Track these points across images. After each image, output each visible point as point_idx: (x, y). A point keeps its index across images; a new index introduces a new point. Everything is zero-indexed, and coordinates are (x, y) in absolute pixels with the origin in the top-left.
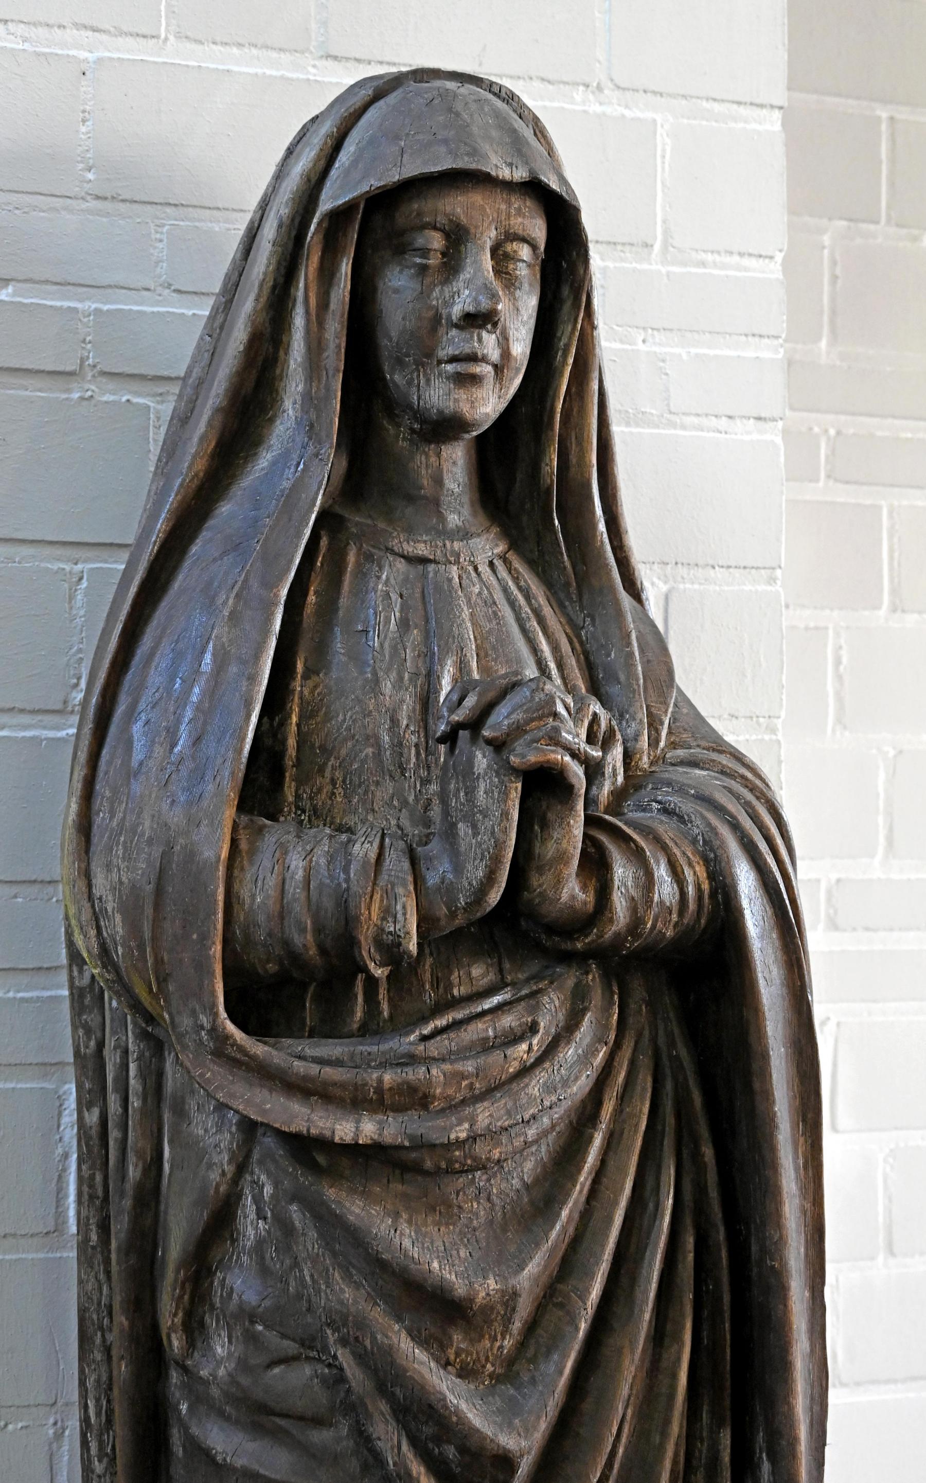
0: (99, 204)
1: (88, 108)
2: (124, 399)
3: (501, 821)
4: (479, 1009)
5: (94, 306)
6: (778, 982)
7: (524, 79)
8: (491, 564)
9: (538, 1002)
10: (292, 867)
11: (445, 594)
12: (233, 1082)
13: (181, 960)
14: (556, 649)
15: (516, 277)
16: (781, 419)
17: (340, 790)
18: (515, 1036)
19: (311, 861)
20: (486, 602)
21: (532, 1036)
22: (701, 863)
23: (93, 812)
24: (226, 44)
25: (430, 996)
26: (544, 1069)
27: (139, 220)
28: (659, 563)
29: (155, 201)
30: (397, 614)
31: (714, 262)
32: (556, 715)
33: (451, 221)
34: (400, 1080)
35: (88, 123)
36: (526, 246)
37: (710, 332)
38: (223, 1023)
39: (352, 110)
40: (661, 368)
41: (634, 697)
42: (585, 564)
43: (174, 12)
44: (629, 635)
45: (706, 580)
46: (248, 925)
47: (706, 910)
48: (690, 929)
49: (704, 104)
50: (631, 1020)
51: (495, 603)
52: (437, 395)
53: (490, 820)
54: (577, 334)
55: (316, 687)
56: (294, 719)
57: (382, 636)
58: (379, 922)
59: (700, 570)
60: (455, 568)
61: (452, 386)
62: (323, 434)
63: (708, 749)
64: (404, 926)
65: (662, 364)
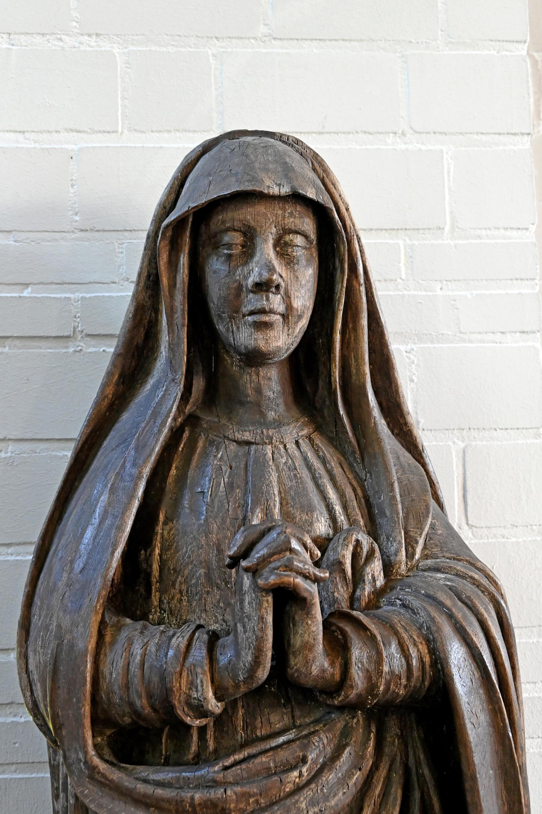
0: (83, 234)
1: (74, 178)
2: (101, 350)
3: (259, 623)
4: (268, 747)
5: (81, 295)
6: (485, 724)
7: (352, 133)
8: (297, 443)
9: (309, 742)
10: (134, 653)
11: (261, 464)
12: (102, 797)
13: (68, 715)
14: (342, 496)
15: (294, 257)
16: (538, 331)
17: (185, 598)
18: (291, 766)
19: (146, 649)
20: (289, 468)
21: (303, 766)
22: (424, 643)
23: (32, 615)
24: (160, 131)
25: (241, 735)
26: (310, 789)
27: (108, 242)
28: (457, 429)
29: (117, 229)
30: (226, 480)
31: (487, 235)
32: (291, 550)
33: (244, 224)
34: (205, 799)
35: (75, 187)
36: (299, 236)
37: (486, 280)
38: (91, 758)
39: (189, 161)
40: (453, 305)
41: (395, 526)
42: (364, 438)
43: (127, 116)
44: (392, 485)
45: (491, 438)
46: (109, 693)
47: (428, 675)
48: (416, 691)
49: (475, 136)
50: (386, 750)
51: (296, 469)
52: (244, 337)
53: (252, 622)
54: (344, 290)
55: (171, 530)
56: (157, 551)
57: (213, 495)
58: (187, 691)
59: (487, 432)
60: (270, 447)
61: (253, 330)
62: (177, 367)
63: (450, 559)
64: (202, 694)
65: (453, 303)
